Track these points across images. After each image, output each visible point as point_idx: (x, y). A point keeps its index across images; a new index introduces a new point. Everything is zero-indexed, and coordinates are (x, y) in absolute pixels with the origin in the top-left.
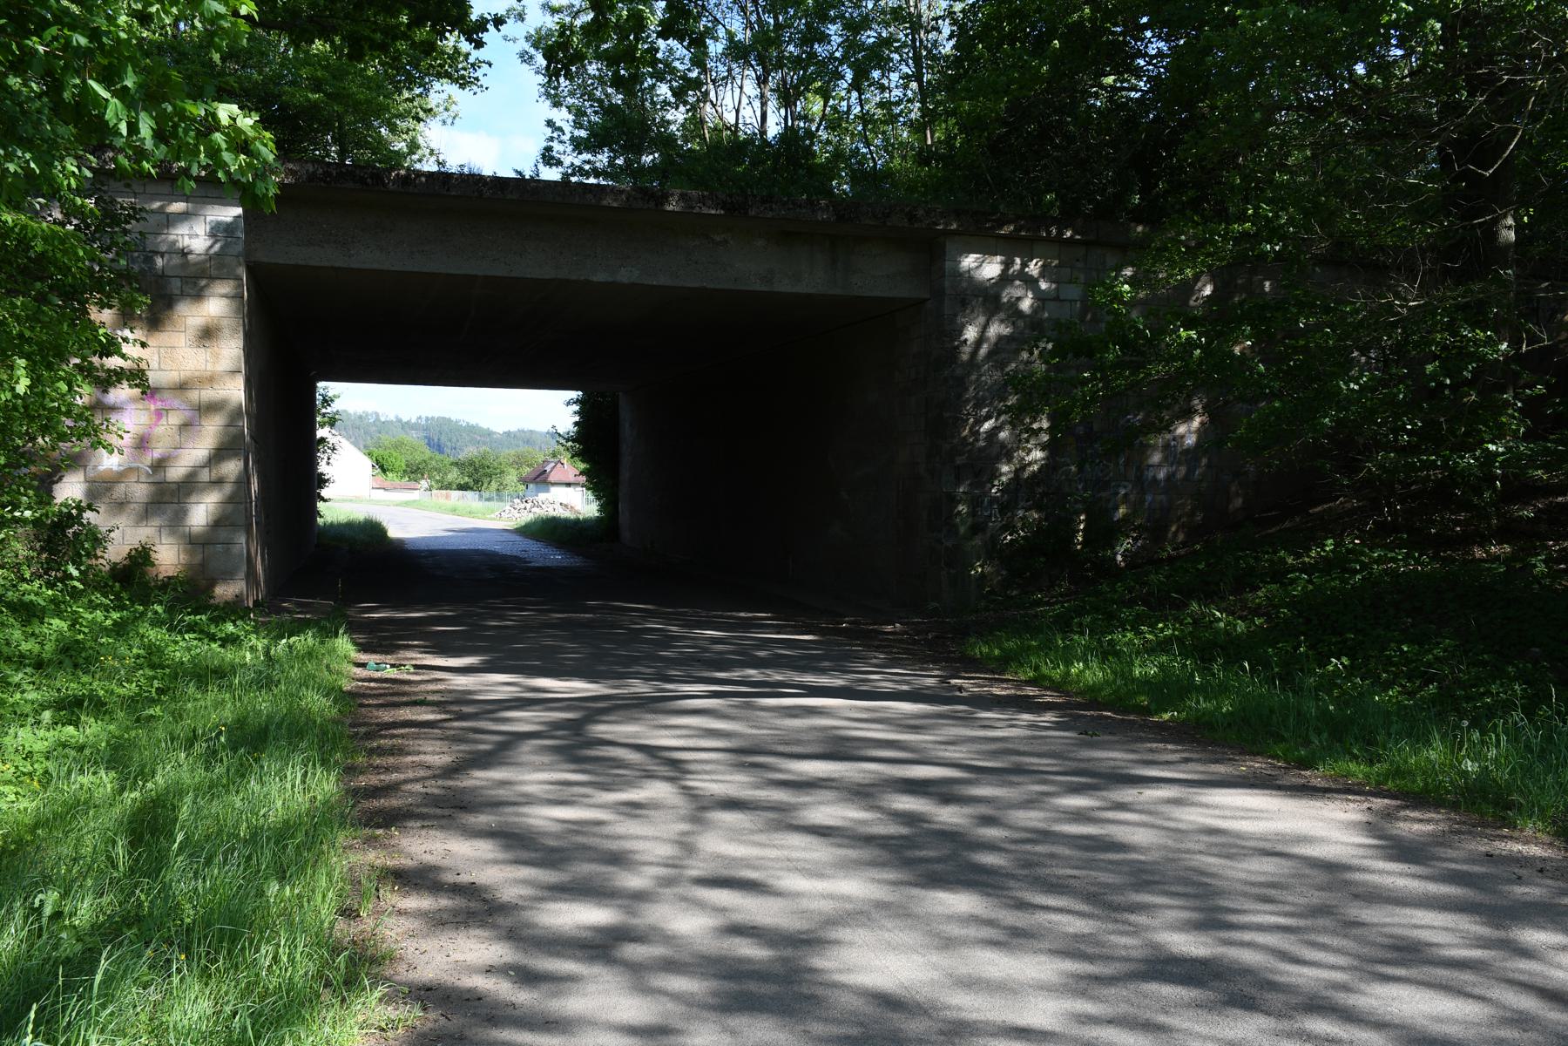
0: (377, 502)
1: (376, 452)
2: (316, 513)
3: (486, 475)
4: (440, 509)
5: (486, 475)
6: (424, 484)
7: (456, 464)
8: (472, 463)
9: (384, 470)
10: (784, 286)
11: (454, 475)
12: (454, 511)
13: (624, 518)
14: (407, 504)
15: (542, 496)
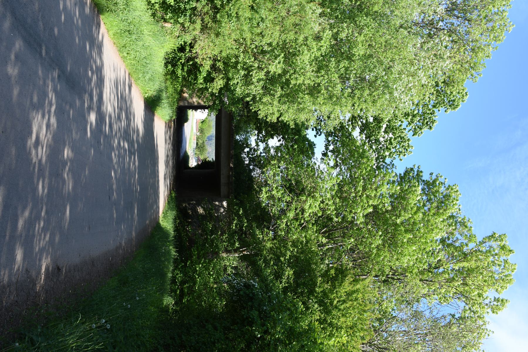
0: (193, 121)
1: (207, 120)
2: (189, 109)
3: (201, 150)
4: (191, 136)
5: (201, 150)
6: (198, 134)
7: (203, 142)
8: (204, 146)
9: (202, 122)
10: (222, 176)
11: (200, 141)
12: (190, 139)
13: (189, 170)
14: (192, 128)
15: (194, 160)
